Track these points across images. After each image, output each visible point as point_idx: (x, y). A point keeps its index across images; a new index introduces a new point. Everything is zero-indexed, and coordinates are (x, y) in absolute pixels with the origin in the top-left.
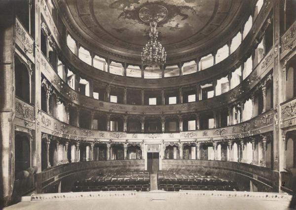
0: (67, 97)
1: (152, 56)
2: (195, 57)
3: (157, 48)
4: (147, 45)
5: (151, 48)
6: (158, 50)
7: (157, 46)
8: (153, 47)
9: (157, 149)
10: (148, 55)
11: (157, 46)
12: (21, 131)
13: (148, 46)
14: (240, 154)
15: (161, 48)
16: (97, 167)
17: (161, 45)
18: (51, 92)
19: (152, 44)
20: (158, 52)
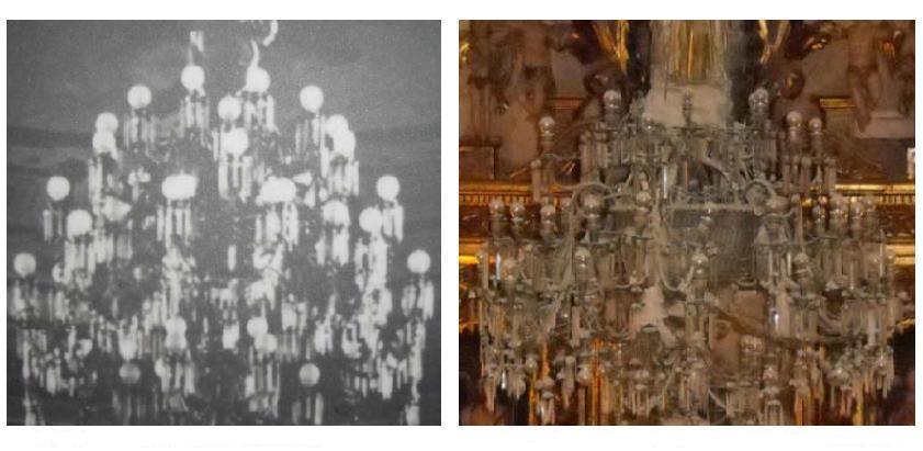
0: (591, 262)
1: (201, 313)
2: (608, 31)
3: (278, 190)
4: (104, 133)
5: (180, 186)
6: (292, 226)
7: (272, 152)
8: (206, 168)
9: (871, 207)
10: (133, 302)
11: (272, 152)
12: (481, 334)
13: (134, 152)
14: (903, 200)
15: (350, 180)
16: (852, 195)
17: (340, 133)
18: (55, 358)
19: (191, 115)
20: (298, 260)
